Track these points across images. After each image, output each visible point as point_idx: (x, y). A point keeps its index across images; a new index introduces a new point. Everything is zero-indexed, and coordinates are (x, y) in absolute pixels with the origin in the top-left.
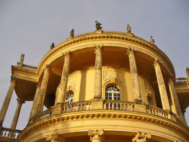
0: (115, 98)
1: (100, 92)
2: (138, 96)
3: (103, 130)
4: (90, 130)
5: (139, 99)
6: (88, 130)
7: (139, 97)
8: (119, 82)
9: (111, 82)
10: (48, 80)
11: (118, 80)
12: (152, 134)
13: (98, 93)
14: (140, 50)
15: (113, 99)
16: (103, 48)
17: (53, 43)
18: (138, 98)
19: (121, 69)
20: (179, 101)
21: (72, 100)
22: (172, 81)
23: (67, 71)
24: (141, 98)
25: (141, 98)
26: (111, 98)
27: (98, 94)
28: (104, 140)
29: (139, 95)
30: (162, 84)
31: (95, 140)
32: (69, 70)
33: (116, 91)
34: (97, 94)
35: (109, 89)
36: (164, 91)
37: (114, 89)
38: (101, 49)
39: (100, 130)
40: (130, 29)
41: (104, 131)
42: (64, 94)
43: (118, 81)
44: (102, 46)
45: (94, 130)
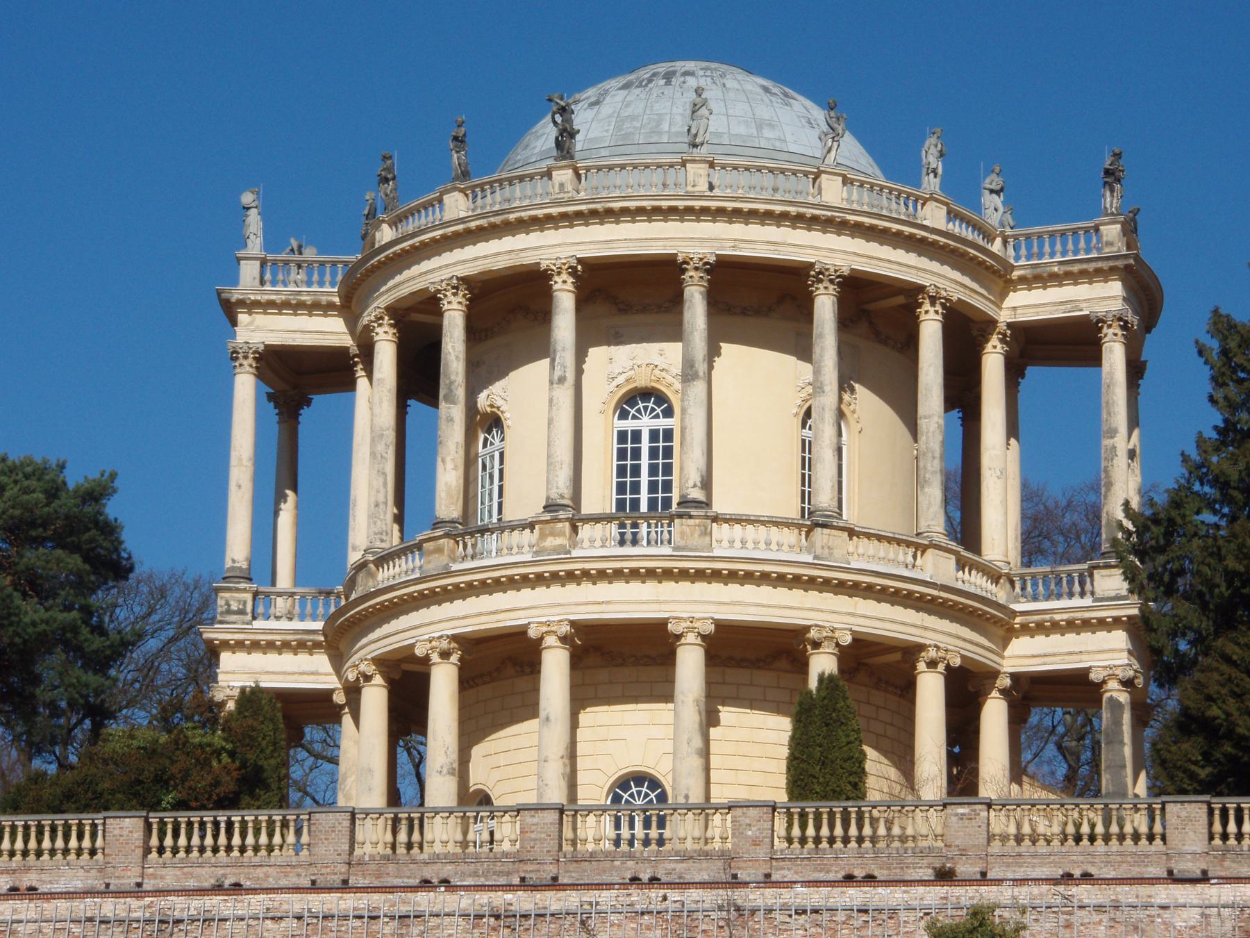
0: (652, 503)
15: (644, 507)
26: (635, 504)
33: (657, 416)
37: (653, 410)
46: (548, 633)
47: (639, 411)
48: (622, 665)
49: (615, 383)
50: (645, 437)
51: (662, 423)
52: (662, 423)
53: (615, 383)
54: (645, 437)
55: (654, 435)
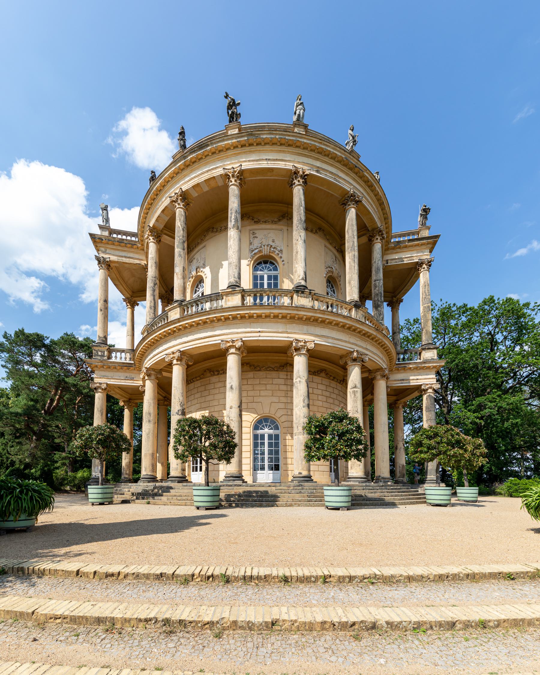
0: (269, 285)
1: (236, 275)
2: (301, 277)
3: (241, 339)
4: (222, 341)
5: (303, 283)
6: (220, 341)
7: (303, 279)
8: (277, 252)
9: (263, 254)
10: (158, 260)
11: (274, 248)
12: (316, 342)
13: (234, 277)
14: (317, 171)
15: (266, 286)
16: (242, 175)
17: (152, 172)
18: (300, 281)
19: (281, 223)
20: (384, 284)
21: (203, 294)
22: (379, 240)
23: (183, 237)
24: (306, 281)
25: (306, 281)
26: (262, 285)
27: (233, 279)
28: (244, 354)
29: (302, 275)
30: (353, 249)
31: (233, 355)
32: (185, 235)
33: (271, 270)
34: (232, 280)
35: (260, 268)
36: (353, 264)
37: (269, 267)
38: (238, 177)
39: (237, 340)
40: (302, 111)
41: (243, 341)
42: (182, 284)
43: (275, 250)
44: (239, 169)
45: (229, 340)
46: (231, 347)
47: (263, 268)
48: (259, 370)
49: (253, 253)
50: (266, 277)
51: (273, 273)
52: (273, 273)
53: (253, 253)
54: (266, 277)
55: (270, 437)
